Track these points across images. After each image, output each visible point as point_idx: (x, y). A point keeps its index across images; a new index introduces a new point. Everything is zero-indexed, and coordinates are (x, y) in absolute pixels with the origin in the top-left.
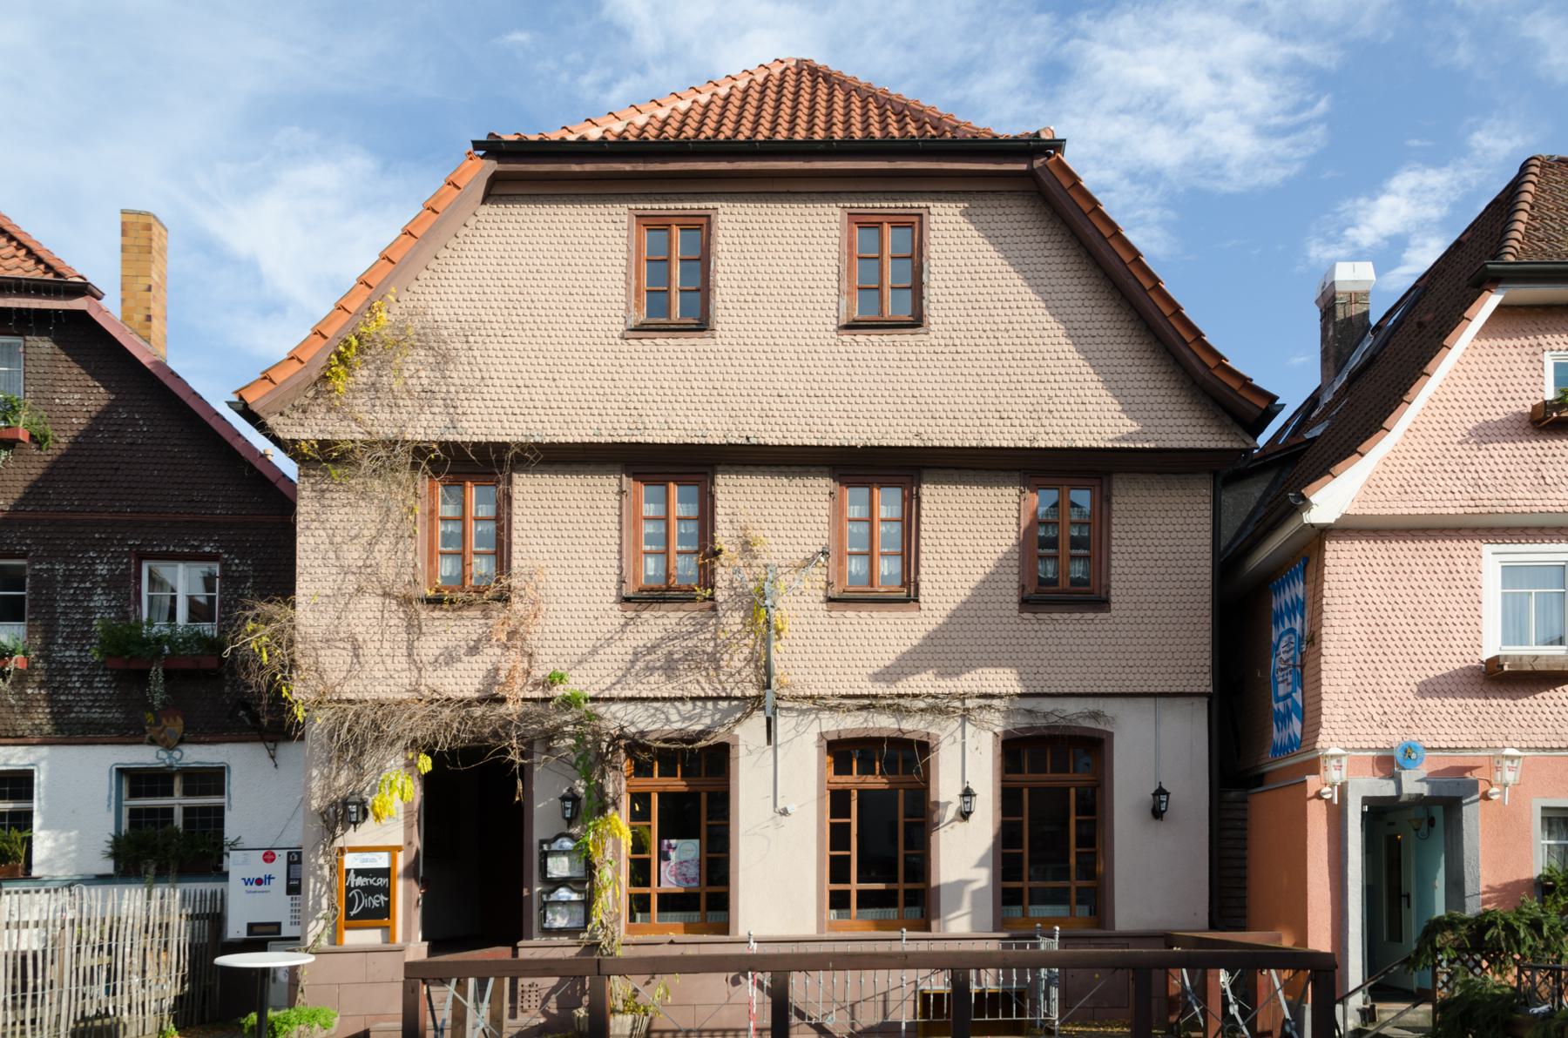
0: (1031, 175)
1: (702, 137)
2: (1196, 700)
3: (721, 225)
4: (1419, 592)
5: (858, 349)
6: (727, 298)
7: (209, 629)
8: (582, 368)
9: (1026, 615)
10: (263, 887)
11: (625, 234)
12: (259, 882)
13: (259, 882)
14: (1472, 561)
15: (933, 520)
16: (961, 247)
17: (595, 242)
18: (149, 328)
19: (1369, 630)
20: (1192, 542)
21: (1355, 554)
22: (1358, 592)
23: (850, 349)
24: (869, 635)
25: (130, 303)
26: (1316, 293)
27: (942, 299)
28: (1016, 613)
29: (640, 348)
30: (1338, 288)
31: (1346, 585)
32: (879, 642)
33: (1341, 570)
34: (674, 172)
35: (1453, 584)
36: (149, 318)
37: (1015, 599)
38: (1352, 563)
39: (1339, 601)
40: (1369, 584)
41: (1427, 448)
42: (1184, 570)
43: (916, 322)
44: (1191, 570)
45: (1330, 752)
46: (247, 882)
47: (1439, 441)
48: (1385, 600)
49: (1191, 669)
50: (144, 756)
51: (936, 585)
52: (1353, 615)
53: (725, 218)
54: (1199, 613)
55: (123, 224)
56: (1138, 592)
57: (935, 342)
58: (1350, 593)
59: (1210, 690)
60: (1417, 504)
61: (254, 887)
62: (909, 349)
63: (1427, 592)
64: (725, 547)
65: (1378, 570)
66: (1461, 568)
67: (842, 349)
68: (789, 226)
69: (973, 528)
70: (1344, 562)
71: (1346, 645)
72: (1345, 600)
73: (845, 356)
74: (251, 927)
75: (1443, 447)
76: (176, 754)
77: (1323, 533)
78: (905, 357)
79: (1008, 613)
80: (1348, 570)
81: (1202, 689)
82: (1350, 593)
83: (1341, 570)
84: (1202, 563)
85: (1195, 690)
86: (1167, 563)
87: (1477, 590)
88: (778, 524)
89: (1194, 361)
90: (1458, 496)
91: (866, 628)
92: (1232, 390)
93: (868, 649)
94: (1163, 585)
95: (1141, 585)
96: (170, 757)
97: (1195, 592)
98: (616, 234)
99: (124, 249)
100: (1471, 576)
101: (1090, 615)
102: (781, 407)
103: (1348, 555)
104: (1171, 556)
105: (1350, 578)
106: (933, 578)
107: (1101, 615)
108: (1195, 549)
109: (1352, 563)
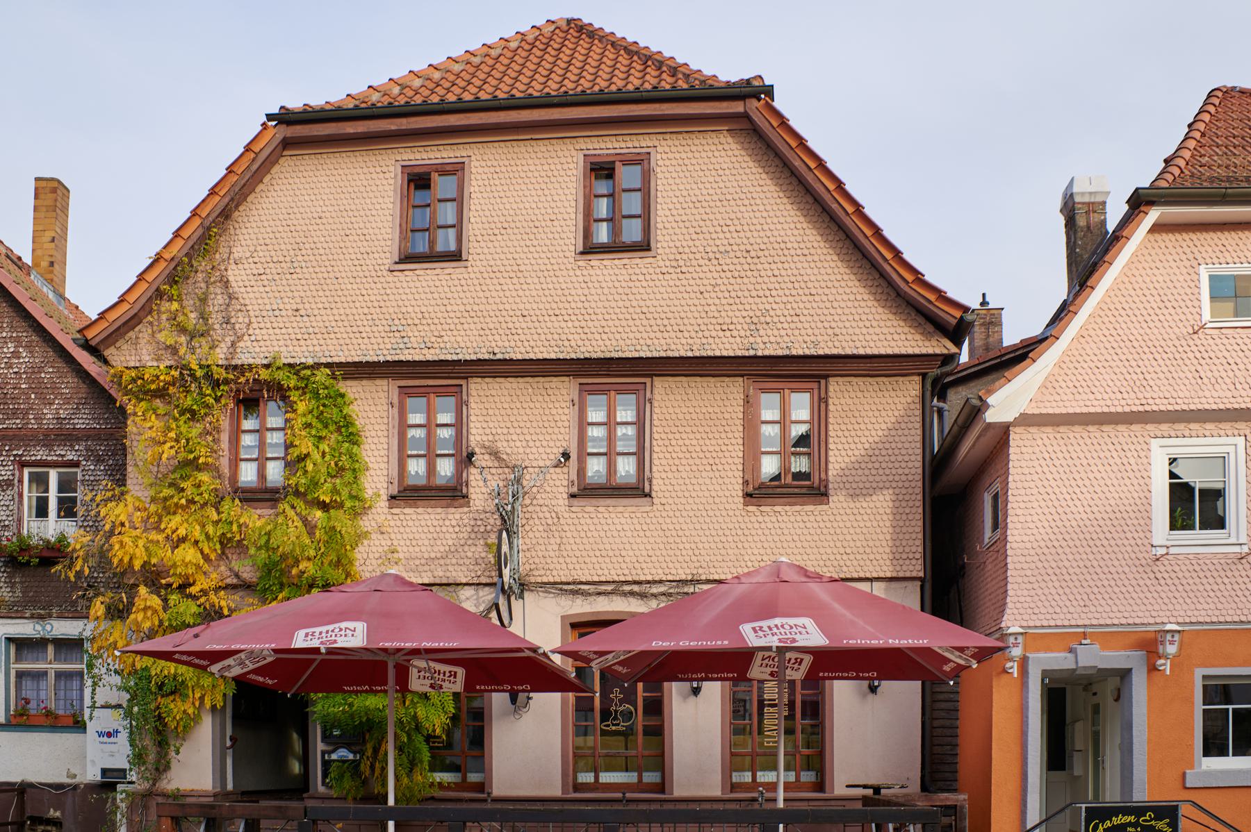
0: (745, 116)
1: (596, 88)
2: (909, 584)
3: (474, 170)
4: (1095, 482)
5: (592, 272)
6: (477, 232)
7: (800, 464)
8: (354, 298)
9: (750, 508)
10: (112, 740)
11: (392, 182)
12: (109, 735)
13: (109, 735)
14: (1142, 454)
15: (664, 423)
16: (696, 178)
17: (364, 190)
18: (52, 272)
19: (1050, 518)
20: (904, 439)
21: (1037, 450)
22: (1039, 484)
23: (585, 272)
24: (606, 528)
25: (39, 252)
26: (1058, 204)
27: (667, 225)
28: (741, 506)
29: (402, 279)
30: (1077, 199)
31: (1029, 478)
32: (615, 534)
33: (1024, 464)
34: (419, 129)
35: (1125, 475)
36: (52, 264)
37: (740, 494)
38: (1033, 457)
39: (1022, 492)
40: (1050, 477)
41: (1098, 352)
42: (897, 465)
43: (644, 247)
44: (903, 464)
45: (1010, 631)
46: (100, 734)
47: (1108, 346)
48: (1064, 490)
49: (904, 556)
50: (25, 628)
51: (667, 482)
52: (1035, 505)
53: (477, 164)
54: (911, 504)
55: (36, 189)
56: (854, 485)
57: (661, 263)
58: (1032, 484)
59: (921, 574)
60: (1088, 403)
61: (105, 739)
62: (637, 271)
63: (1102, 482)
64: (477, 450)
65: (1057, 463)
66: (1132, 461)
67: (578, 272)
68: (533, 168)
69: (701, 429)
70: (1027, 457)
71: (1029, 532)
72: (1029, 492)
73: (581, 279)
74: (105, 772)
75: (1112, 351)
76: (48, 628)
77: (1003, 432)
78: (634, 278)
79: (734, 507)
80: (1030, 464)
81: (914, 574)
82: (1032, 484)
83: (1024, 464)
84: (913, 458)
85: (908, 574)
86: (881, 459)
87: (1147, 480)
88: (523, 427)
89: (894, 276)
90: (1125, 395)
91: (603, 521)
92: (930, 302)
93: (605, 540)
94: (878, 479)
95: (857, 479)
96: (44, 629)
97: (907, 484)
98: (385, 182)
99: (36, 209)
100: (1141, 468)
101: (811, 508)
102: (524, 325)
103: (1030, 450)
104: (884, 452)
105: (1032, 471)
106: (664, 475)
107: (820, 507)
108: (907, 445)
109: (1033, 457)
